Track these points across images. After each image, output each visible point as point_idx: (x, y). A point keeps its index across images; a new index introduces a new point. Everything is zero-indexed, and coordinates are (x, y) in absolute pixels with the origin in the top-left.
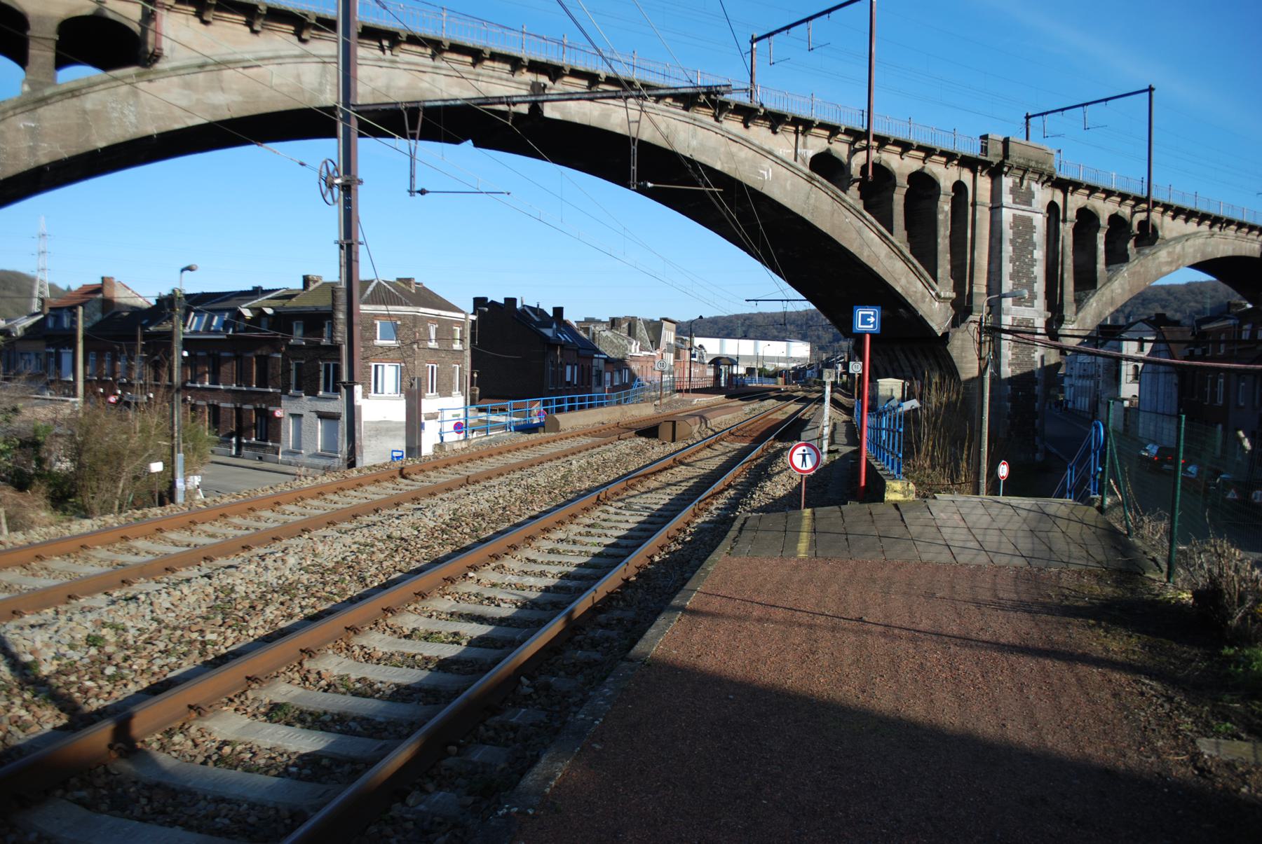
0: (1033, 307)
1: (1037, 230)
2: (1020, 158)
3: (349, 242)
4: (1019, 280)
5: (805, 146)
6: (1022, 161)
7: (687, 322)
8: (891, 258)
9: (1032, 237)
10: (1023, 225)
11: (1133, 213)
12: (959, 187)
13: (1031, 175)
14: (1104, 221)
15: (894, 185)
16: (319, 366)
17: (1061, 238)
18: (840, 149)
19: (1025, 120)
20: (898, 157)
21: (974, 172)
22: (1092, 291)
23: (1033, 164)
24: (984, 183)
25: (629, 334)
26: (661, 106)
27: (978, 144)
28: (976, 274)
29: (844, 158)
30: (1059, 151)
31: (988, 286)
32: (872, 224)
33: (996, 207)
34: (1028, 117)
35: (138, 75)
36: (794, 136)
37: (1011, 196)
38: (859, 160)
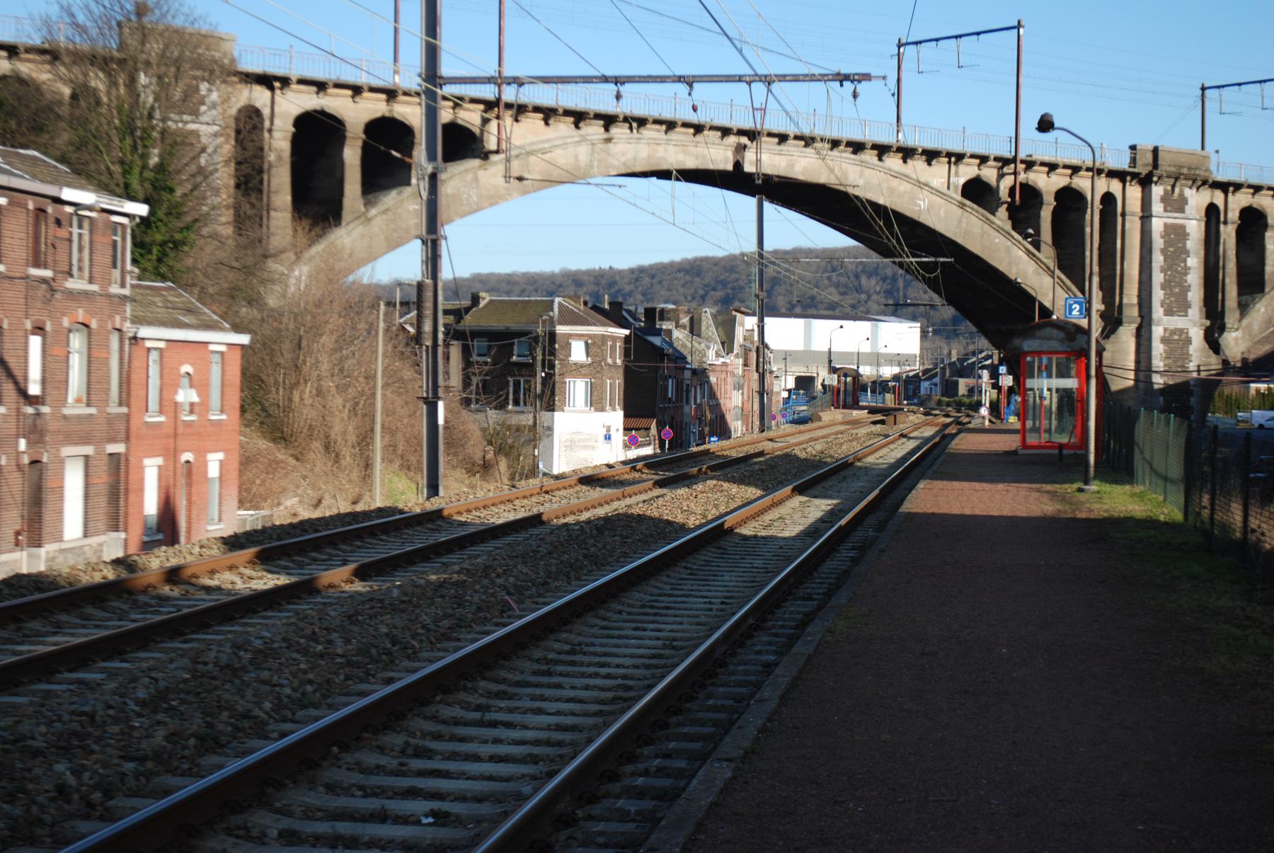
0: (1186, 316)
1: (1190, 237)
2: (1170, 166)
3: (434, 237)
4: (1171, 290)
5: (957, 174)
6: (1172, 169)
7: (632, 271)
8: (1039, 274)
9: (1185, 244)
10: (1176, 235)
12: (1108, 199)
13: (1183, 182)
15: (1041, 203)
16: (508, 382)
17: (1222, 241)
19: (1200, 92)
20: (1045, 175)
21: (1124, 182)
22: (1260, 296)
23: (1185, 171)
24: (1134, 192)
25: (692, 331)
26: (835, 153)
28: (1126, 285)
29: (993, 182)
30: (1217, 152)
31: (1139, 296)
32: (1020, 243)
33: (1146, 217)
34: (1203, 89)
35: (480, 167)
36: (947, 166)
37: (1162, 205)
38: (1007, 182)
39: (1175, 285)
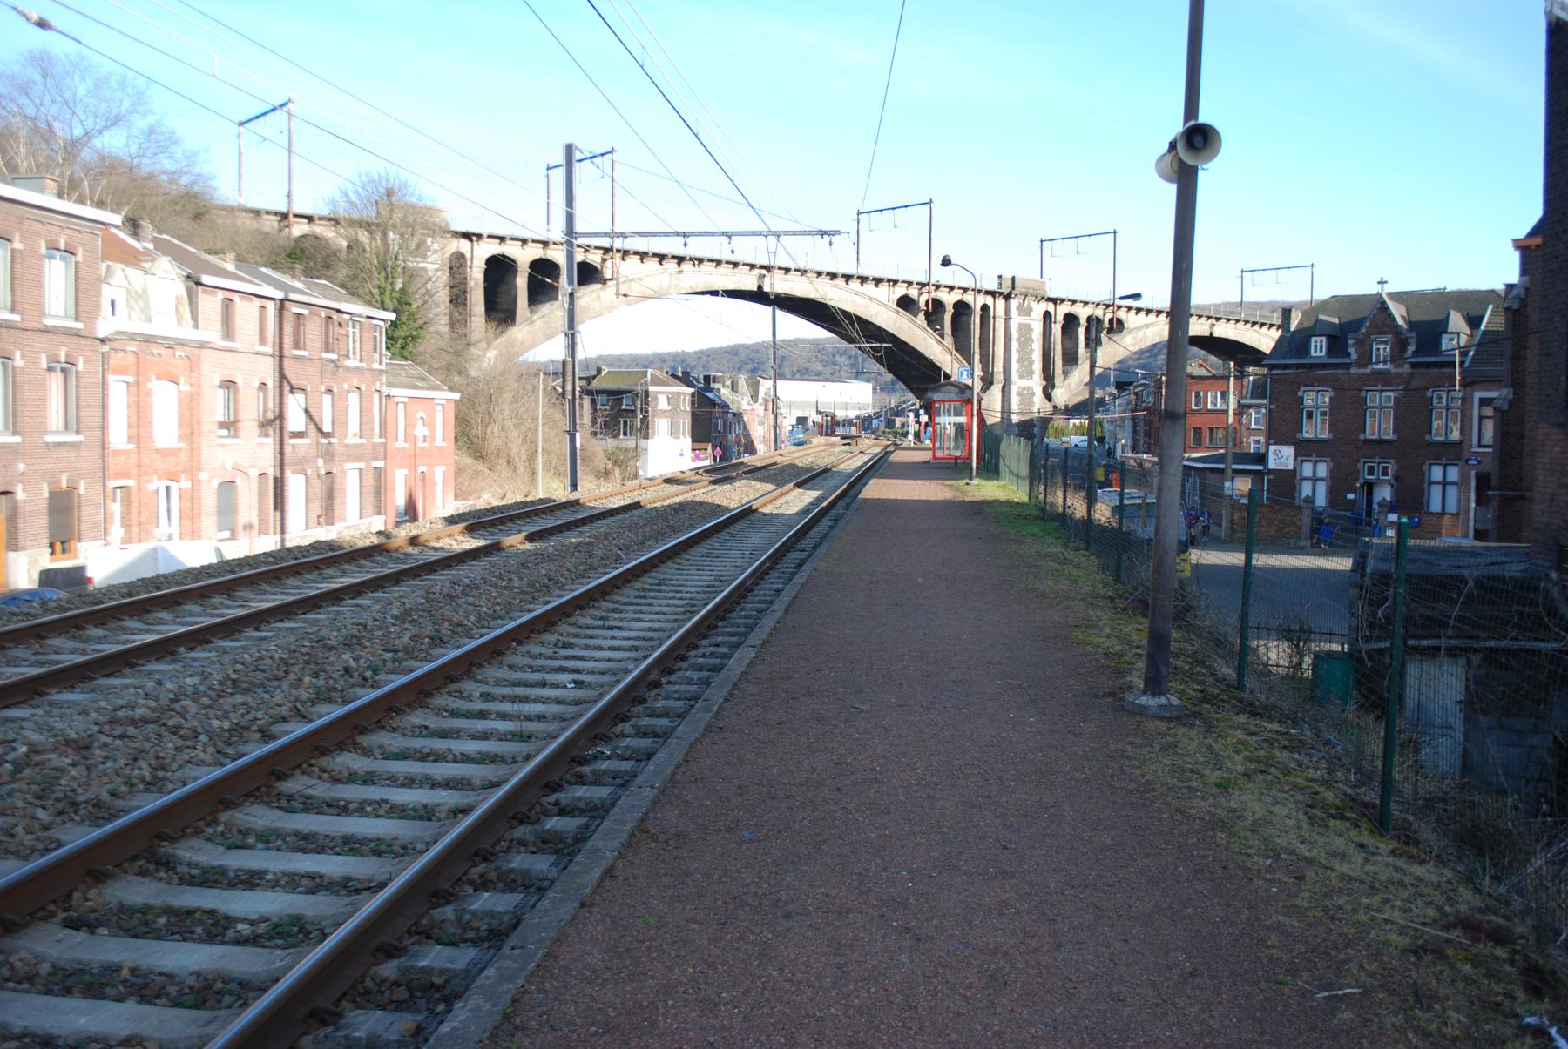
10: (1026, 330)
11: (1105, 314)
14: (1083, 321)
18: (913, 292)
21: (994, 297)
27: (996, 281)
31: (1004, 367)
33: (1008, 319)
38: (1109, 316)
39: (1025, 360)
